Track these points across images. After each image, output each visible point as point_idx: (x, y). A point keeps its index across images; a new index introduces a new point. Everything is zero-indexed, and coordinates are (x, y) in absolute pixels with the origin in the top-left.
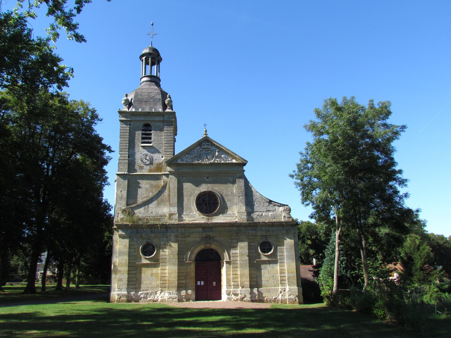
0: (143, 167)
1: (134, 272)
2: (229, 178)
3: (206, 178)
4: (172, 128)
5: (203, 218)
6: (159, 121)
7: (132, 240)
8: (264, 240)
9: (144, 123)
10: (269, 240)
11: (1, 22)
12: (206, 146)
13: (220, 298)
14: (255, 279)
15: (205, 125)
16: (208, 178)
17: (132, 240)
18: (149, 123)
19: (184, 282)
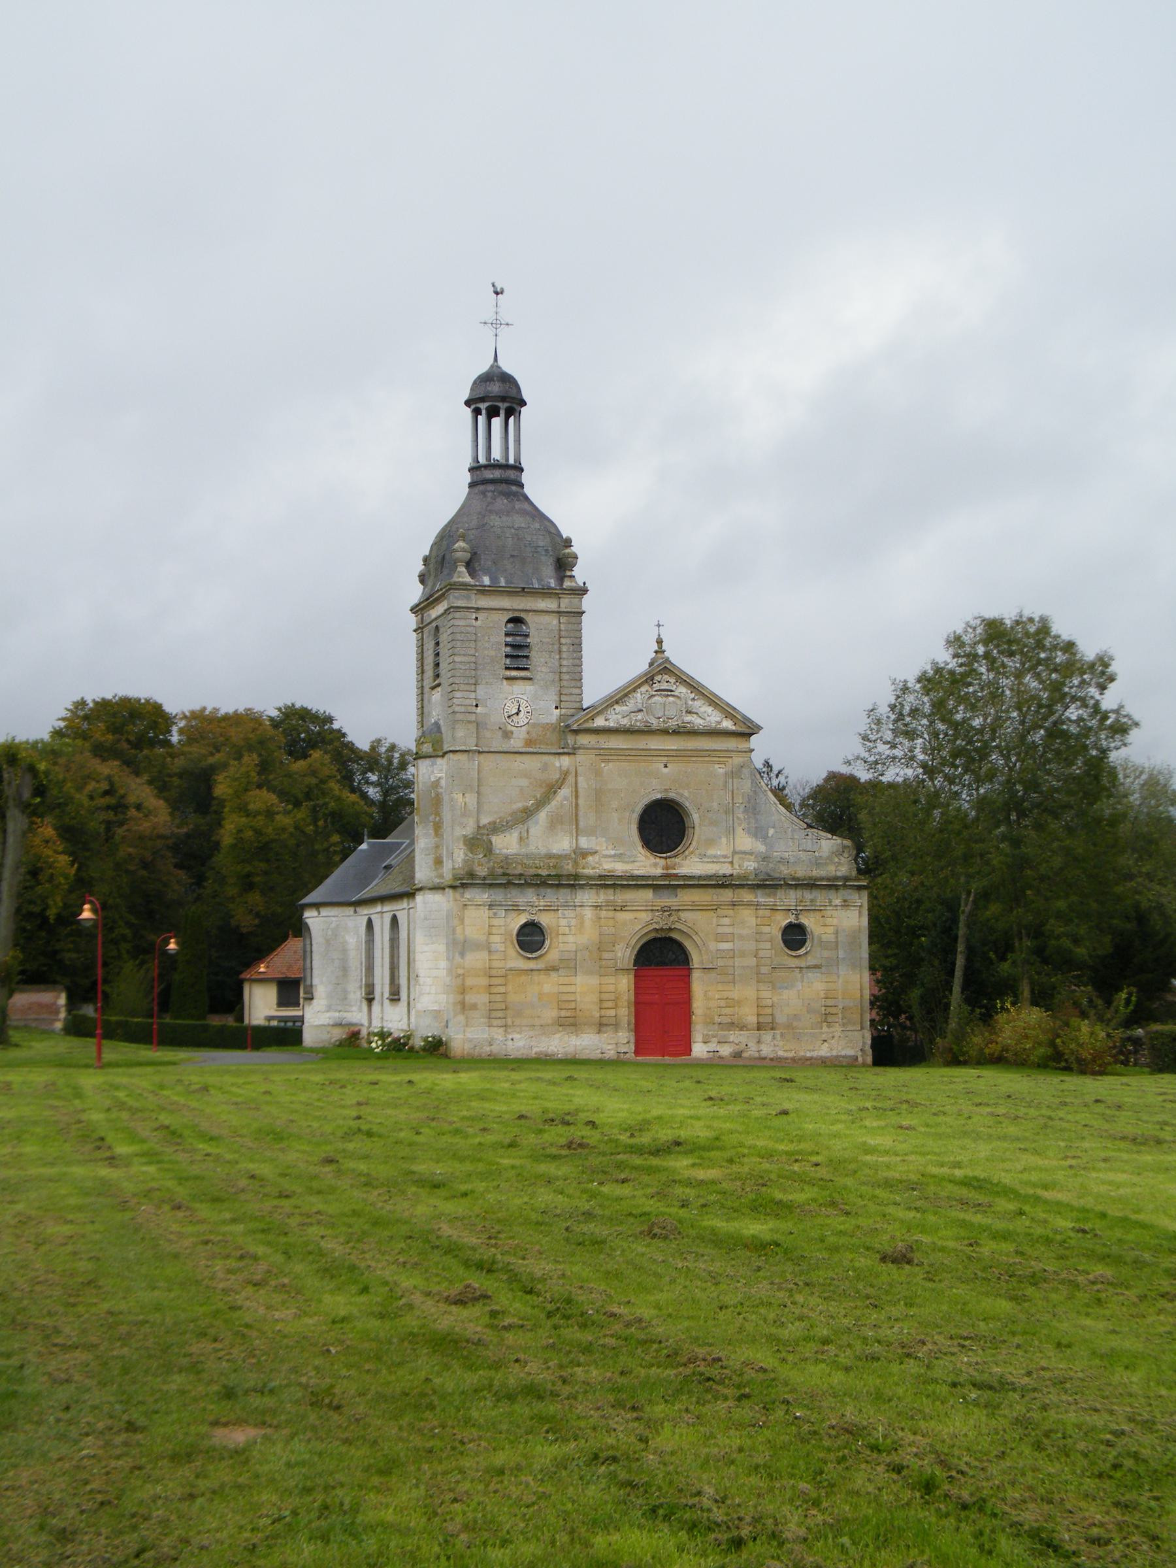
0: (349, 1370)
1: (502, 989)
2: (717, 766)
3: (662, 765)
4: (796, 800)
5: (655, 865)
6: (520, 1082)
7: (495, 914)
8: (791, 919)
9: (511, 615)
10: (805, 920)
11: (1175, 1058)
12: (665, 686)
13: (688, 1051)
14: (769, 1011)
15: (659, 625)
16: (666, 766)
17: (495, 914)
18: (522, 615)
19: (612, 1013)
